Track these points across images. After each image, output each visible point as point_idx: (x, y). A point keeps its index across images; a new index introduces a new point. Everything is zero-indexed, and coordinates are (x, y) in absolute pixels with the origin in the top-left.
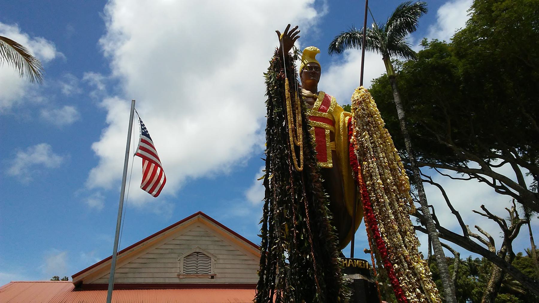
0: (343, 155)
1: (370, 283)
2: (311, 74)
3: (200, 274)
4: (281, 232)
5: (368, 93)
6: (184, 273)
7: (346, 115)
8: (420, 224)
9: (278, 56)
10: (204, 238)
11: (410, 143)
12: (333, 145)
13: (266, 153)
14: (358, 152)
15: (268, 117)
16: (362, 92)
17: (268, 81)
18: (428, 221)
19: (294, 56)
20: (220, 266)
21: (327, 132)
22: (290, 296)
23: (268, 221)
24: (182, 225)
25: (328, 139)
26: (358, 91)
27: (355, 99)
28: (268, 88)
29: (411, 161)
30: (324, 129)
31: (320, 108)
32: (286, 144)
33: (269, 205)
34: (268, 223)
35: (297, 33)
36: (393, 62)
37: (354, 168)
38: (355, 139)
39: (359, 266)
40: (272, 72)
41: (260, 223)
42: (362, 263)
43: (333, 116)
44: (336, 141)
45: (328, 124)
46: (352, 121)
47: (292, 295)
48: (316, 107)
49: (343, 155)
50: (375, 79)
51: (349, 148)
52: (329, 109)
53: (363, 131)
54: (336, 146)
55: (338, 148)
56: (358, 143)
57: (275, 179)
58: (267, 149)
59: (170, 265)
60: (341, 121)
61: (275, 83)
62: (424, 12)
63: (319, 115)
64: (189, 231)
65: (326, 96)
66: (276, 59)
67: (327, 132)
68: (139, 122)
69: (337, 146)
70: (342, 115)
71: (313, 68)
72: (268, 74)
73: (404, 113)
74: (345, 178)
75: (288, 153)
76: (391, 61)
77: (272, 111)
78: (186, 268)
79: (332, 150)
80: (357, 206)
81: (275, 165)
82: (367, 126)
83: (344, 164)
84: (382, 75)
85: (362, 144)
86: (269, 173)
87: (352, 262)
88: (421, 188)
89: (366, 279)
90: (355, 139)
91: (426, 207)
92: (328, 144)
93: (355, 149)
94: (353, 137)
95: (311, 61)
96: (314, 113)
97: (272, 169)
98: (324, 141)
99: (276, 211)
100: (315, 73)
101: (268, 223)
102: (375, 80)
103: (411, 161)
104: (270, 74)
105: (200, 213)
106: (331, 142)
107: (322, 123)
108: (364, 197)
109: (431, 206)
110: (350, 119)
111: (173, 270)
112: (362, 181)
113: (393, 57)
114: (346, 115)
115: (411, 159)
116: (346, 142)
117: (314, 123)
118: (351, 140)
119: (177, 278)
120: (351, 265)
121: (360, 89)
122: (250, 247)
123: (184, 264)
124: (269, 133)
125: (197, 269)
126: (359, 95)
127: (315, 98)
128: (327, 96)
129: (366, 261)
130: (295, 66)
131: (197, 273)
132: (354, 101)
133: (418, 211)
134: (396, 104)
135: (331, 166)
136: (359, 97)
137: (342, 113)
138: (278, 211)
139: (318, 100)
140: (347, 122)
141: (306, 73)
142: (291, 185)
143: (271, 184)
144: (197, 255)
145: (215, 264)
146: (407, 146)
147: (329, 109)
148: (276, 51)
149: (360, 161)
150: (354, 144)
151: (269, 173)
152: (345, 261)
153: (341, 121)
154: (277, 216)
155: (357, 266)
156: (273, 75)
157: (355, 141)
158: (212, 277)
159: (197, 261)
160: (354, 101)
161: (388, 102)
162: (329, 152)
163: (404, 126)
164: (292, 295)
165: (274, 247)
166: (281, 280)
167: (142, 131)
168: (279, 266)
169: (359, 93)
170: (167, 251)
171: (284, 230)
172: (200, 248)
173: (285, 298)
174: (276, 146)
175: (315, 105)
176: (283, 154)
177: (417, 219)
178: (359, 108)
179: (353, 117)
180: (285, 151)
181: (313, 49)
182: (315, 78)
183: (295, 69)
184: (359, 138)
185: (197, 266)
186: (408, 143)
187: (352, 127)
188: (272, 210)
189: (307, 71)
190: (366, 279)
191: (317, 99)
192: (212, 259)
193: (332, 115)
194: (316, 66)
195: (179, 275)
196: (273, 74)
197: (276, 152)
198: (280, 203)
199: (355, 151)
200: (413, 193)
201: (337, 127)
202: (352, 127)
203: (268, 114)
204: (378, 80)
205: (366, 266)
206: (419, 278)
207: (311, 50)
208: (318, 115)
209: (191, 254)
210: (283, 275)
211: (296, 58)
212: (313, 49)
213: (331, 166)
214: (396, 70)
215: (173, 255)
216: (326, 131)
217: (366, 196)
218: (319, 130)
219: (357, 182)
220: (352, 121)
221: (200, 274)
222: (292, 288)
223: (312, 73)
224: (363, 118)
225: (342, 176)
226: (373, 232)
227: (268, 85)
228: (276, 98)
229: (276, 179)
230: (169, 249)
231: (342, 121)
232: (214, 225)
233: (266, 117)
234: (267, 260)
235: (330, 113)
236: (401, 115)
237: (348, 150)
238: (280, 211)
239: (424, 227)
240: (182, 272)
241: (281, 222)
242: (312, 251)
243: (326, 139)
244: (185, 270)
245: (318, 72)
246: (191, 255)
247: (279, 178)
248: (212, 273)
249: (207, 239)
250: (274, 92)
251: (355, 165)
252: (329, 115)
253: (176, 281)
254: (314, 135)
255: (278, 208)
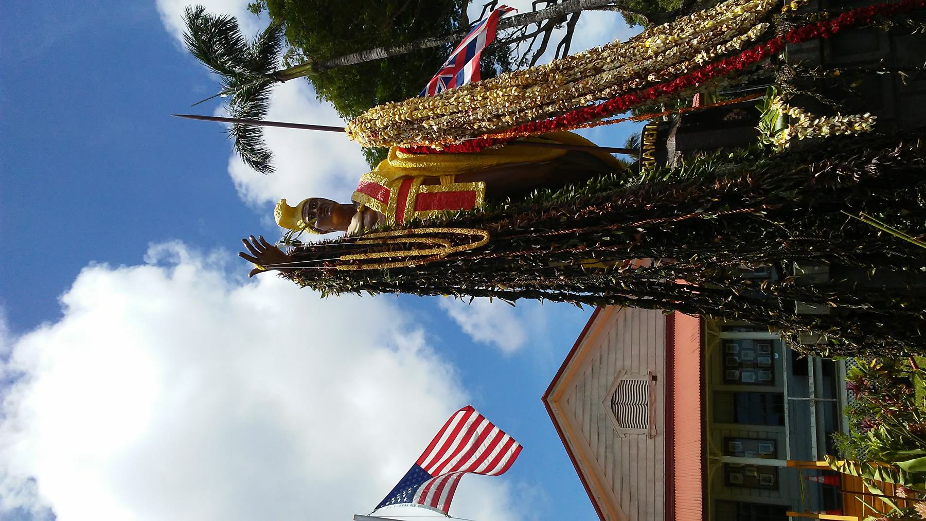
0: (464, 163)
1: (681, 123)
2: (323, 215)
3: (649, 398)
4: (598, 274)
5: (357, 120)
6: (647, 428)
7: (394, 157)
8: (565, 24)
9: (293, 274)
10: (588, 393)
11: (429, 40)
12: (446, 179)
13: (461, 296)
14: (458, 138)
15: (398, 291)
16: (355, 129)
17: (335, 290)
18: (561, 12)
19: (294, 245)
20: (636, 363)
21: (424, 189)
22: (708, 261)
23: (577, 294)
24: (565, 430)
25: (436, 189)
26: (354, 136)
27: (367, 142)
28: (347, 290)
29: (459, 38)
30: (419, 196)
31: (382, 202)
32: (447, 262)
33: (549, 291)
34: (581, 294)
35: (255, 241)
36: (288, 64)
37: (487, 145)
38: (437, 143)
39: (654, 141)
40: (320, 284)
41: (582, 308)
42: (648, 135)
43: (397, 179)
44: (439, 174)
45: (409, 188)
46: (404, 147)
47: (706, 258)
48: (380, 208)
49: (464, 163)
50: (317, 95)
51: (452, 153)
52: (384, 185)
53: (423, 129)
54: (447, 175)
55: (451, 171)
56: (443, 138)
57: (507, 281)
58: (453, 294)
59: (634, 451)
60: (405, 166)
61: (341, 279)
62: (202, 11)
63: (394, 202)
64: (575, 417)
65: (361, 190)
66: (298, 276)
67: (424, 189)
68: (391, 507)
69: (448, 173)
70: (394, 164)
71: (312, 211)
72: (324, 290)
73: (377, 48)
74: (503, 160)
75: (461, 260)
76: (285, 68)
77: (388, 285)
78: (636, 424)
79: (456, 182)
80: (549, 141)
81: (481, 283)
82: (414, 124)
83: (478, 162)
84: (309, 83)
85: (446, 132)
86: (495, 290)
87: (646, 153)
88: (505, 22)
89: (675, 130)
90: (437, 143)
91: (538, 14)
92: (444, 188)
93: (454, 143)
94: (433, 147)
95: (300, 215)
96: (390, 211)
97: (488, 286)
98: (438, 195)
99: (562, 280)
100: (321, 209)
101: (581, 294)
102: (319, 95)
103: (459, 38)
104: (325, 288)
105: (545, 399)
106: (440, 184)
107: (408, 199)
108: (536, 130)
109: (534, 4)
110: (402, 150)
111: (642, 446)
112: (509, 133)
113: (280, 63)
114: (394, 157)
115: (456, 39)
116: (440, 157)
117: (408, 212)
118: (438, 149)
119: (656, 439)
120: (651, 155)
121: (351, 133)
122: (603, 313)
123: (634, 427)
124: (426, 290)
125: (641, 405)
126: (360, 134)
127: (364, 209)
128: (360, 188)
129: (645, 129)
130: (310, 244)
131: (647, 405)
132: (370, 142)
133: (541, 27)
134: (362, 61)
135: (482, 185)
136: (364, 134)
137: (390, 163)
138: (562, 278)
139: (367, 205)
140: (406, 156)
141: (319, 225)
142: (518, 256)
143: (514, 288)
144: (617, 404)
145: (631, 374)
146: (434, 45)
147: (384, 185)
148: (284, 276)
149: (473, 135)
150: (445, 145)
151: (495, 290)
152: (645, 165)
153: (405, 166)
154: (571, 280)
155: (654, 144)
156: (326, 282)
157: (440, 144)
158: (654, 378)
159: (627, 404)
160: (370, 142)
161: (357, 74)
162: (458, 187)
163: (399, 48)
164: (706, 258)
165: (623, 286)
166: (681, 275)
167: (406, 502)
168: (656, 279)
169: (356, 133)
170: (610, 455)
171: (594, 269)
172: (605, 399)
173: (712, 270)
174: (449, 279)
175: (376, 210)
176: (464, 267)
177: (557, 28)
178: (383, 134)
179: (399, 145)
180: (458, 265)
181: (279, 212)
182: (329, 210)
183: (317, 245)
184: (434, 136)
185: (630, 404)
186: (428, 43)
187: (415, 147)
188: (559, 287)
189: (316, 222)
190: (675, 130)
191: (366, 205)
192: (623, 379)
193: (394, 181)
194: (308, 206)
195: (651, 437)
196: (324, 283)
197: (459, 279)
198: (548, 273)
199: (457, 143)
200: (512, 35)
201: (414, 173)
202: (415, 147)
203: (392, 292)
204: (319, 89)
205: (653, 130)
206: (674, 44)
207: (280, 214)
208: (395, 205)
209: (615, 415)
210: (673, 272)
211: (297, 243)
212: (280, 211)
213: (482, 185)
214: (303, 58)
215: (617, 446)
216: (422, 191)
217: (535, 126)
218: (420, 203)
219: (511, 142)
220: (404, 147)
221: (649, 398)
222: (694, 258)
223: (320, 213)
224: (400, 129)
225: (498, 165)
226: (592, 116)
227: (342, 291)
228: (366, 278)
229: (505, 280)
230: (606, 452)
231: (404, 164)
232: (565, 374)
233: (398, 296)
234: (646, 298)
235: (390, 184)
236: (380, 54)
237: (455, 154)
238: (561, 275)
239: (569, 17)
240: (646, 431)
241: (581, 273)
242: (632, 224)
243: (436, 193)
244: (639, 425)
245: (319, 203)
246: (617, 414)
247: (504, 275)
248: (647, 378)
249: (588, 387)
250: (355, 281)
251: (481, 144)
252: (394, 185)
253: (661, 440)
254: (428, 211)
255: (557, 278)
